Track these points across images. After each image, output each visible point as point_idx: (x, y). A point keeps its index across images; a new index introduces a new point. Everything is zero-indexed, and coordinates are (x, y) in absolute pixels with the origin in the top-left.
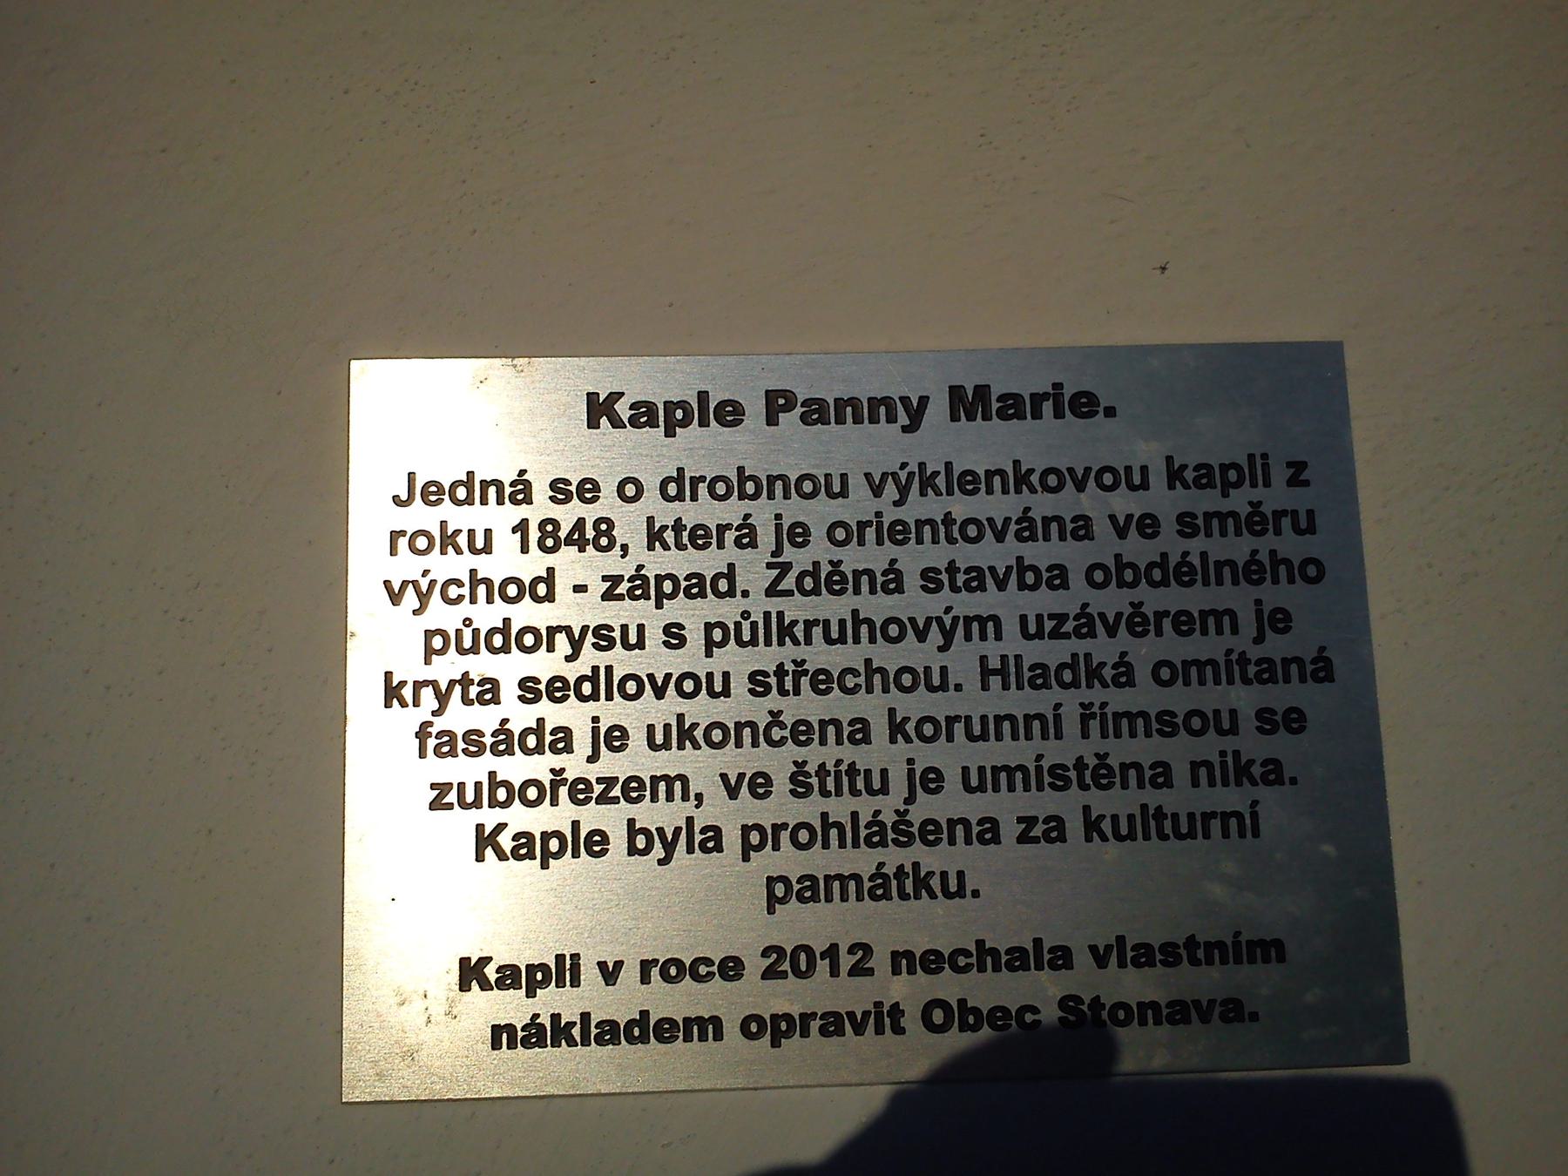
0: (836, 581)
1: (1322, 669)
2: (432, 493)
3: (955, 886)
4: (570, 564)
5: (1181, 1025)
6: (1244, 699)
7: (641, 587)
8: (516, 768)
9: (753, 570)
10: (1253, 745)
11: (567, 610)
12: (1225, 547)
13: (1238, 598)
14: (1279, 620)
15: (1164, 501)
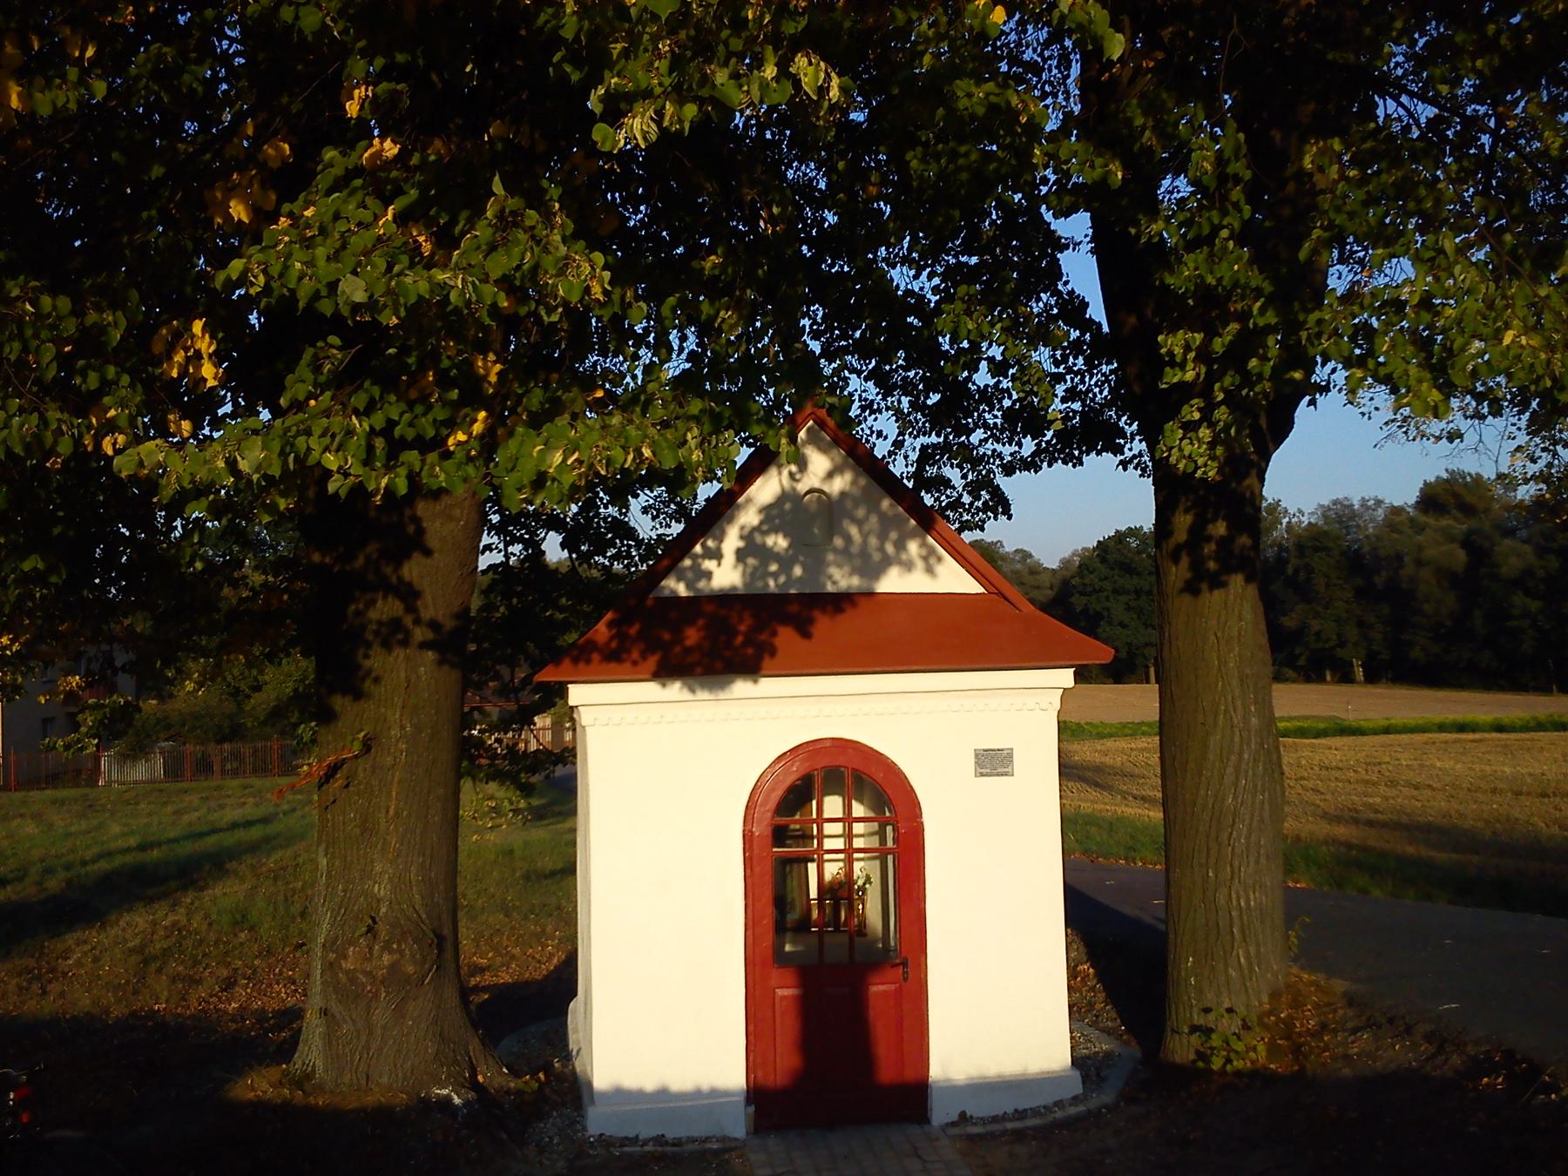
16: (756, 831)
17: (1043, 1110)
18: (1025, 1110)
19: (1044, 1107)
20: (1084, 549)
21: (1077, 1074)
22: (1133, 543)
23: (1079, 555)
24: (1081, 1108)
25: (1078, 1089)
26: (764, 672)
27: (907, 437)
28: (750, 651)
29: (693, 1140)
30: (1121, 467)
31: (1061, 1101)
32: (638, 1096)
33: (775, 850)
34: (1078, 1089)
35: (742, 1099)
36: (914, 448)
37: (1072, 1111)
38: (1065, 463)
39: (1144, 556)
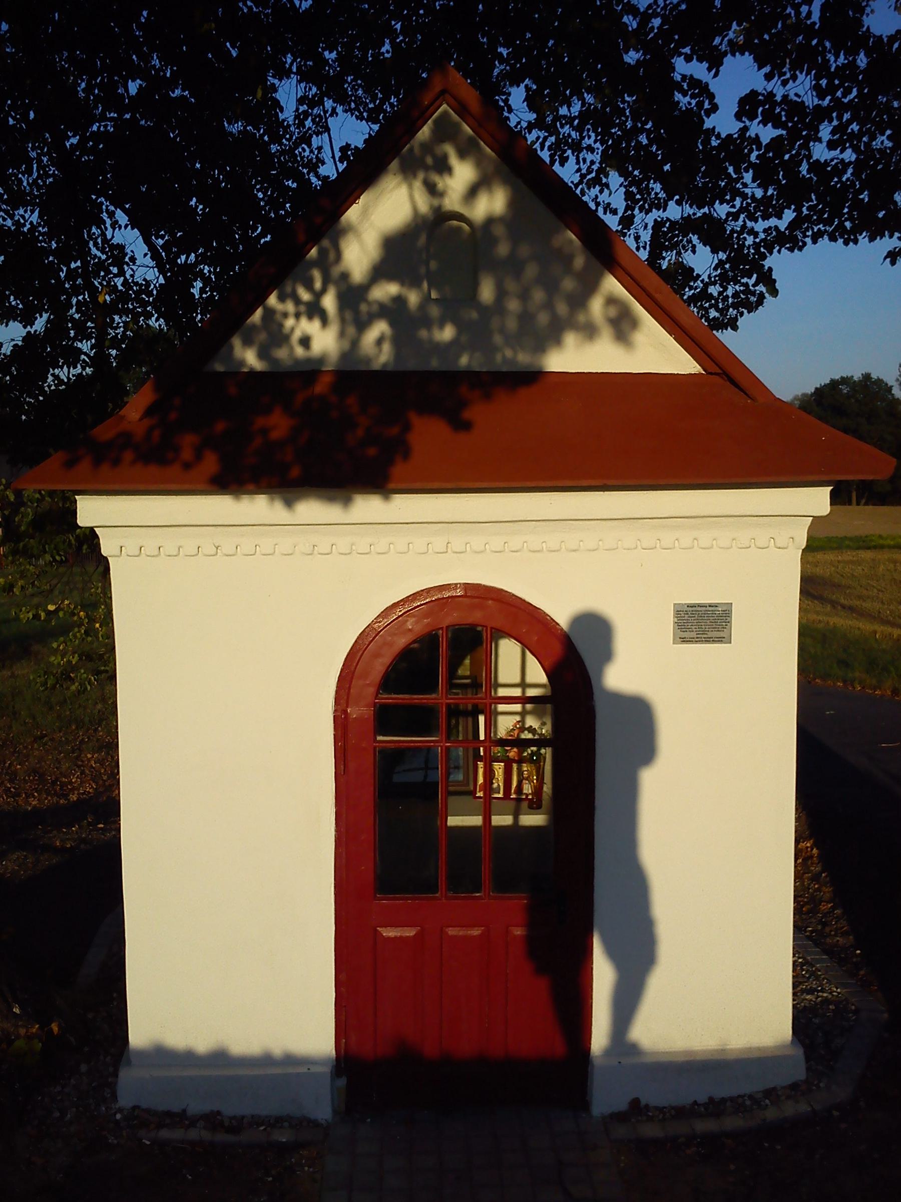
0: (701, 617)
1: (729, 622)
2: (678, 611)
3: (707, 634)
4: (686, 615)
5: (894, 33)
6: (724, 624)
7: (689, 617)
8: (683, 627)
9: (696, 616)
10: (724, 626)
11: (686, 618)
12: (724, 615)
13: (724, 618)
14: (726, 619)
15: (721, 612)
16: (353, 712)
17: (748, 1103)
18: (723, 1100)
19: (751, 1097)
20: (804, 395)
21: (799, 1052)
22: (845, 389)
23: (799, 399)
24: (803, 1107)
25: (800, 1074)
26: (392, 486)
27: (636, 211)
28: (372, 451)
29: (256, 1121)
30: (888, 260)
31: (774, 1089)
32: (188, 1058)
33: (380, 738)
34: (800, 1074)
35: (327, 1069)
36: (646, 225)
37: (790, 1109)
38: (833, 239)
39: (853, 401)
